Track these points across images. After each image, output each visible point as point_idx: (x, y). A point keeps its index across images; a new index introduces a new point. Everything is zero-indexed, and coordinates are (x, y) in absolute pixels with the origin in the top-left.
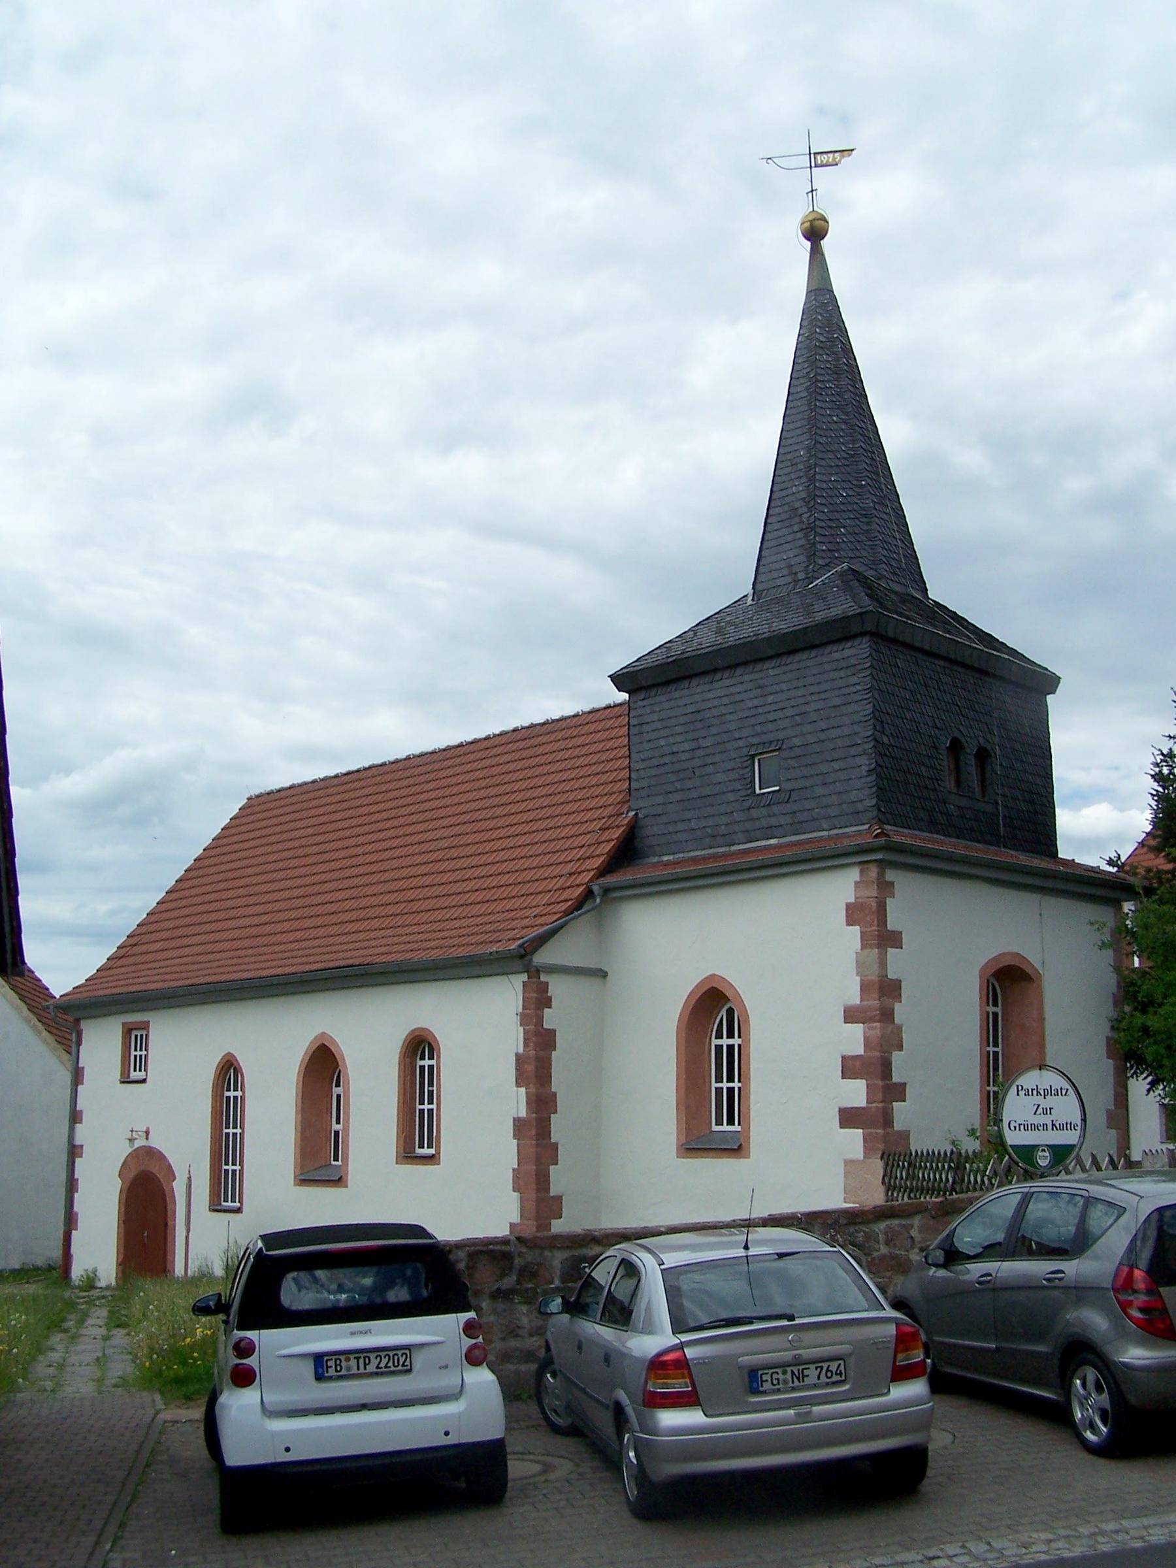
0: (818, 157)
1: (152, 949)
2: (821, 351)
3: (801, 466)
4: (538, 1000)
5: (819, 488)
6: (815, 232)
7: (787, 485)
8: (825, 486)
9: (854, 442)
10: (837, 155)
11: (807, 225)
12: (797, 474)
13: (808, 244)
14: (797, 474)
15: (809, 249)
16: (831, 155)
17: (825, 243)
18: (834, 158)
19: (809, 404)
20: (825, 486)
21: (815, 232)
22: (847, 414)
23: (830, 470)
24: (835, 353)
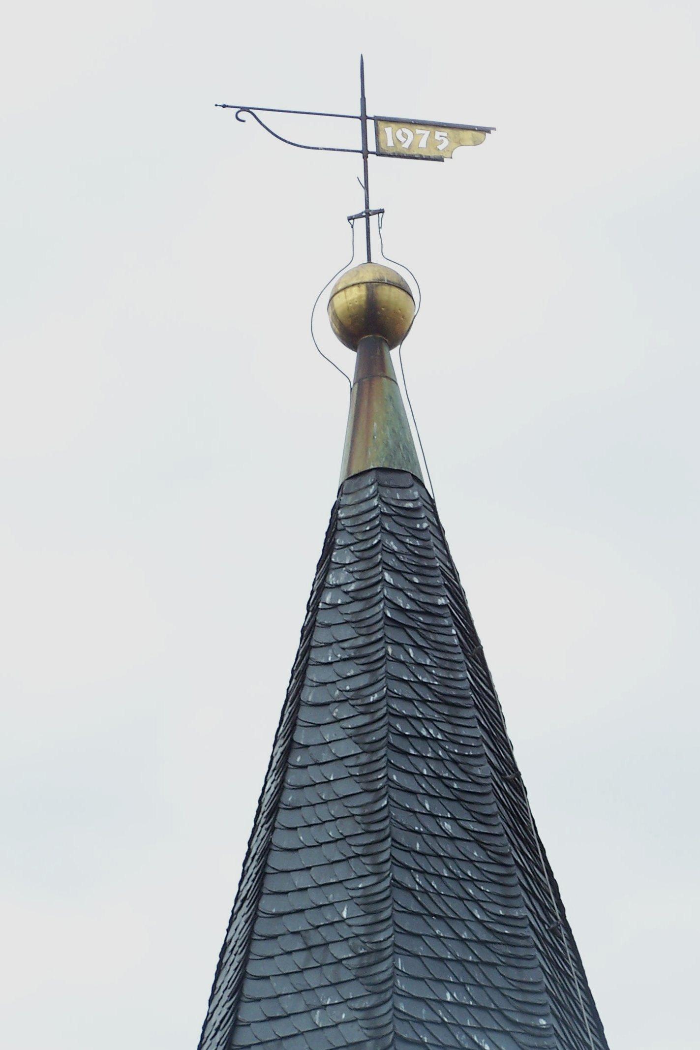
0: (388, 131)
1: (374, 621)
2: (399, 636)
3: (340, 951)
4: (367, 206)
5: (408, 1019)
6: (373, 327)
7: (289, 1004)
8: (424, 1013)
9: (508, 900)
10: (439, 134)
11: (357, 295)
12: (330, 974)
13: (348, 359)
14: (330, 974)
15: (351, 372)
16: (425, 132)
17: (403, 359)
18: (431, 141)
19: (366, 776)
20: (424, 1013)
21: (373, 327)
22: (483, 819)
23: (437, 970)
24: (439, 647)
